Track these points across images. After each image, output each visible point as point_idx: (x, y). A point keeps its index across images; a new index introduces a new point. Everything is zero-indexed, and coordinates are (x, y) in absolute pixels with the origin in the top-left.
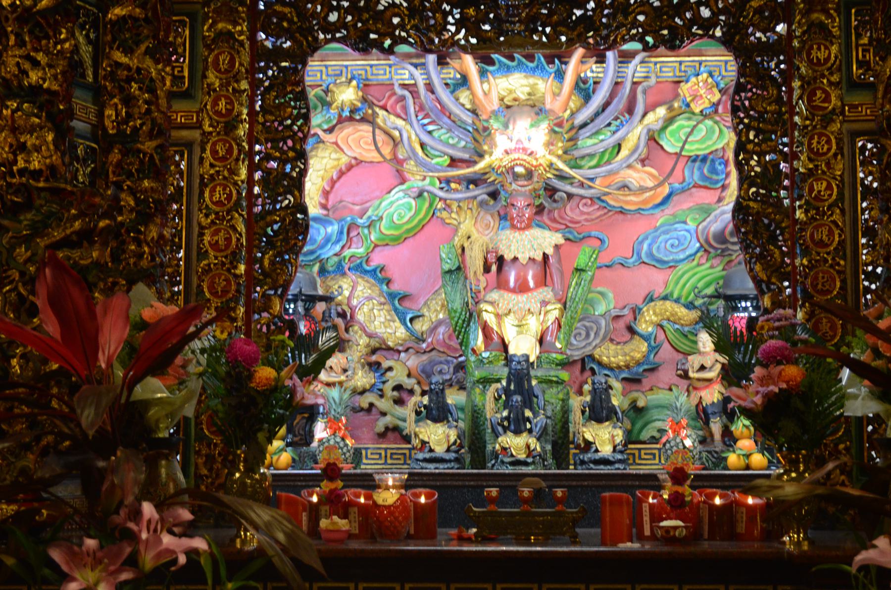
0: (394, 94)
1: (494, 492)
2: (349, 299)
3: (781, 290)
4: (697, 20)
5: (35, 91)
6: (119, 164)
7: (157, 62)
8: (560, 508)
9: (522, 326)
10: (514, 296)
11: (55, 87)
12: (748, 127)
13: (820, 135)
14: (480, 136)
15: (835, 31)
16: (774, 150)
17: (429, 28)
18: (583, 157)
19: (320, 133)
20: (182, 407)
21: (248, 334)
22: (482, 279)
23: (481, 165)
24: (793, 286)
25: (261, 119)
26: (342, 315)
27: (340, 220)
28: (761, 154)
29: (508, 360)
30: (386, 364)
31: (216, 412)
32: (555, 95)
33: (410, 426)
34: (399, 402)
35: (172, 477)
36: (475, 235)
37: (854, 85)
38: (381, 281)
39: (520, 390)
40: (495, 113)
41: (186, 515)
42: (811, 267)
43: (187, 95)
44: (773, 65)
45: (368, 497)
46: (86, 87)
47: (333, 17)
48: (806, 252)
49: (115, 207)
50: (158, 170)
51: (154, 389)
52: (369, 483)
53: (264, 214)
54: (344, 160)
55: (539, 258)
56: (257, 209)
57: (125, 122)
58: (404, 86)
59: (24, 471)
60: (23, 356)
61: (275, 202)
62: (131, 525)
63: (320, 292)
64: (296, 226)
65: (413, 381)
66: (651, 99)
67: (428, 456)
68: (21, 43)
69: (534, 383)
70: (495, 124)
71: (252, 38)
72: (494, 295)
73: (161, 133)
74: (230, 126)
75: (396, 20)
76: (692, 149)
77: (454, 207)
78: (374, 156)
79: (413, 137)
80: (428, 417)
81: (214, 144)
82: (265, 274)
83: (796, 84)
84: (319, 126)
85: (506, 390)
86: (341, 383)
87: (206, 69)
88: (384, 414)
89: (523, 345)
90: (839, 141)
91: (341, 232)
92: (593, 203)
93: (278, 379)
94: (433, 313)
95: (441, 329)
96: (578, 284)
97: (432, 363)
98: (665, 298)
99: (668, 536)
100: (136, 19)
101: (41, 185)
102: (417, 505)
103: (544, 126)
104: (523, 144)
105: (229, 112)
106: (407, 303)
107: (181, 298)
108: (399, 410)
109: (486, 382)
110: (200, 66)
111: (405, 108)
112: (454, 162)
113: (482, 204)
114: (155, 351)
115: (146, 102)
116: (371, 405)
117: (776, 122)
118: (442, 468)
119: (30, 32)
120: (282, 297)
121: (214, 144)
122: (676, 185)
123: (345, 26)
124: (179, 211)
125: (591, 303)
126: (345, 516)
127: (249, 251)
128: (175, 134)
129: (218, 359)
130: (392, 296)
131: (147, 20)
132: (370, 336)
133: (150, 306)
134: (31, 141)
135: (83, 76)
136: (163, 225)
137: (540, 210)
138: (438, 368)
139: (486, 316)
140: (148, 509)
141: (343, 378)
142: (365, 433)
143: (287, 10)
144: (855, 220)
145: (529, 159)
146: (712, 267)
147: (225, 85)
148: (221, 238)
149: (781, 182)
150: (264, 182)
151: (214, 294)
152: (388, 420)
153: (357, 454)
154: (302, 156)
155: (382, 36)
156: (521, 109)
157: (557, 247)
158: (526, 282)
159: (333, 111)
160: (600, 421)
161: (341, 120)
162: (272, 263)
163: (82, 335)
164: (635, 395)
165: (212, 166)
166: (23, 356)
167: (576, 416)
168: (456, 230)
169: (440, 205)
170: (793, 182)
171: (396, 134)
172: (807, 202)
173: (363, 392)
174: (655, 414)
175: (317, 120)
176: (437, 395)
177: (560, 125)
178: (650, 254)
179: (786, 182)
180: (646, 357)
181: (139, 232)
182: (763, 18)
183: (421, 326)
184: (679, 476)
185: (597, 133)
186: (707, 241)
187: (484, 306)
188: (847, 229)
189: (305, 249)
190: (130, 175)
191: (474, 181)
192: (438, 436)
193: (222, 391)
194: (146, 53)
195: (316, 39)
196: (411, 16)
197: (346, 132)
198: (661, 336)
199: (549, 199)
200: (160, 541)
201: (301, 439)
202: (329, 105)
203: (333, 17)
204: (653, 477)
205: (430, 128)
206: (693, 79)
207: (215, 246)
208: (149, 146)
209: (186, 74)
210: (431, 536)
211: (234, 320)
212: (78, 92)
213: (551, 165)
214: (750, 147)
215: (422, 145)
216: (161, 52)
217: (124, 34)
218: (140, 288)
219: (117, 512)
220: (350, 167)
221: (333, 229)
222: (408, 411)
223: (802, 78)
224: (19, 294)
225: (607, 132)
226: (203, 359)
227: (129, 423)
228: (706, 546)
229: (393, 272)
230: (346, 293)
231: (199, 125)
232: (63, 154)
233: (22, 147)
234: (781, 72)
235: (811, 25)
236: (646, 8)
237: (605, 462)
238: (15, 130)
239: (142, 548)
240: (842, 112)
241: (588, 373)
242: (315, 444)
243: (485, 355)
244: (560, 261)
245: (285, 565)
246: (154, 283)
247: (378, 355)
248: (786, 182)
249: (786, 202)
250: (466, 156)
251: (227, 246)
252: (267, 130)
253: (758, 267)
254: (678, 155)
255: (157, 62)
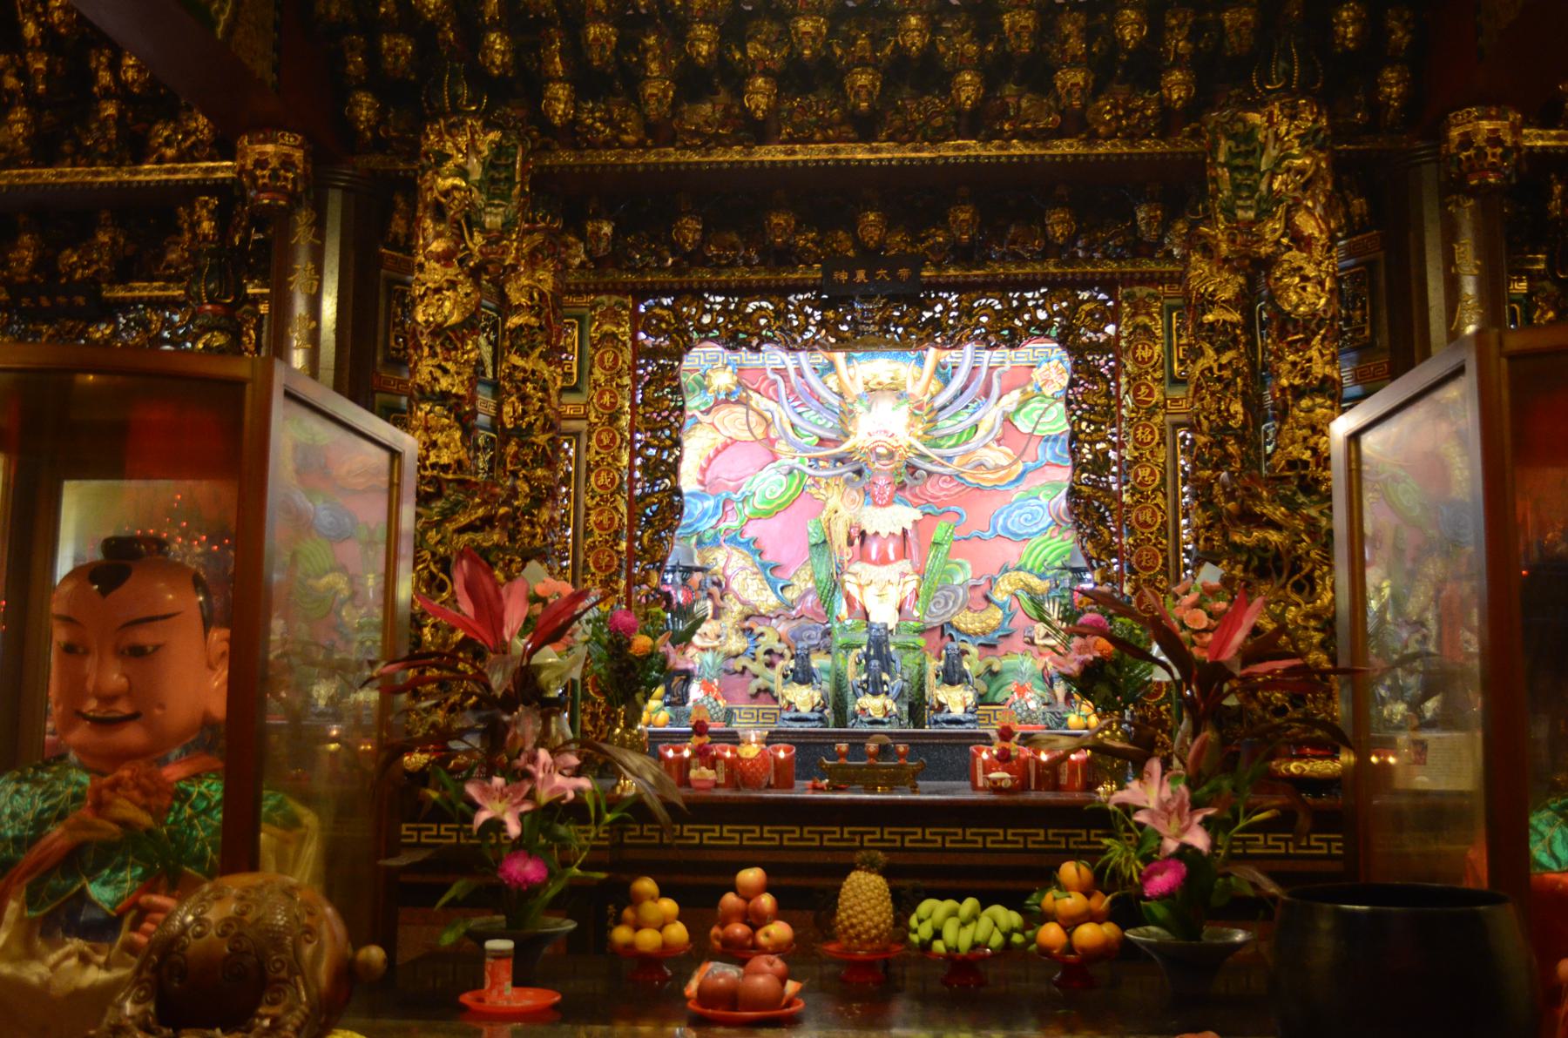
0: (767, 378)
1: (844, 747)
2: (724, 568)
3: (1109, 566)
4: (1034, 321)
5: (444, 397)
6: (516, 455)
7: (550, 364)
8: (902, 761)
9: (882, 594)
10: (875, 568)
11: (462, 392)
12: (1081, 419)
13: (1145, 426)
14: (845, 416)
15: (1159, 333)
16: (1103, 440)
17: (792, 329)
18: (942, 437)
19: (698, 414)
20: (570, 670)
21: (629, 604)
22: (847, 550)
23: (843, 448)
24: (1121, 563)
25: (641, 411)
26: (718, 584)
27: (716, 495)
28: (1093, 443)
29: (870, 627)
30: (758, 630)
31: (599, 675)
32: (916, 380)
33: (778, 687)
34: (770, 665)
35: (560, 732)
36: (842, 511)
37: (1176, 381)
38: (754, 552)
39: (879, 656)
40: (859, 397)
41: (573, 760)
42: (1136, 546)
43: (575, 389)
44: (1102, 362)
45: (733, 751)
46: (485, 383)
47: (706, 320)
48: (1132, 532)
49: (514, 493)
50: (548, 460)
51: (548, 655)
52: (733, 739)
53: (644, 496)
54: (720, 440)
55: (899, 532)
56: (638, 492)
57: (522, 417)
58: (776, 371)
59: (434, 725)
60: (434, 626)
61: (653, 485)
62: (530, 767)
63: (697, 563)
64: (672, 505)
65: (783, 646)
66: (1006, 382)
67: (794, 715)
68: (434, 355)
69: (892, 648)
70: (859, 408)
71: (634, 338)
72: (857, 567)
73: (552, 427)
74: (614, 418)
75: (763, 322)
76: (1043, 430)
77: (823, 483)
78: (746, 436)
79: (785, 418)
80: (794, 680)
81: (599, 434)
82: (644, 550)
83: (1123, 380)
84: (697, 408)
85: (867, 656)
86: (714, 649)
87: (592, 366)
88: (756, 676)
89: (884, 614)
90: (1162, 431)
91: (717, 507)
92: (952, 479)
93: (653, 647)
94: (802, 582)
95: (810, 598)
96: (935, 557)
97: (802, 629)
98: (1019, 569)
99: (995, 788)
100: (532, 327)
101: (450, 476)
102: (776, 759)
103: (905, 409)
104: (883, 426)
105: (613, 404)
106: (778, 573)
107: (569, 572)
108: (769, 673)
109: (848, 647)
110: (587, 363)
111: (776, 391)
112: (822, 442)
113: (847, 481)
114: (551, 626)
115: (540, 400)
116: (745, 668)
117: (1106, 414)
118: (806, 727)
119: (442, 344)
120: (659, 570)
121: (599, 434)
122: (1030, 464)
123: (717, 327)
124: (568, 494)
125: (951, 574)
126: (714, 767)
127: (630, 530)
128: (566, 425)
129: (601, 628)
130: (764, 566)
131: (541, 328)
132: (744, 603)
133: (539, 579)
134: (441, 438)
135: (484, 373)
136: (554, 509)
137: (902, 486)
138: (807, 634)
139: (848, 586)
140: (543, 754)
141: (716, 643)
142: (739, 694)
143: (665, 313)
144: (1176, 503)
145: (890, 440)
146: (1063, 540)
147: (609, 381)
148: (605, 518)
149: (1109, 470)
150: (644, 468)
151: (599, 568)
152: (759, 682)
153: (729, 714)
154: (677, 443)
155: (751, 335)
156: (883, 391)
157: (915, 522)
158: (886, 554)
159: (710, 396)
160: (952, 684)
161: (717, 403)
162: (651, 540)
163: (490, 612)
164: (990, 659)
165: (597, 453)
166: (434, 626)
167: (931, 680)
168: (823, 506)
169: (810, 481)
170: (1120, 469)
171: (768, 415)
172: (1133, 487)
173: (736, 656)
174: (1009, 677)
175: (694, 403)
176: (803, 659)
177: (920, 408)
178: (1005, 528)
179: (1115, 469)
180: (1001, 624)
181: (533, 515)
182: (1094, 320)
183: (790, 595)
184: (1006, 734)
185: (956, 414)
186: (1058, 516)
187: (846, 577)
188: (1170, 512)
189: (684, 522)
190: (525, 465)
191: (841, 460)
192: (803, 698)
193: (605, 657)
194: (541, 356)
195: (691, 339)
196: (777, 318)
197: (722, 414)
198: (1015, 604)
199: (909, 477)
200: (552, 780)
201: (677, 700)
202: (707, 388)
203: (706, 320)
204: (986, 736)
205: (800, 410)
206: (1045, 365)
207: (599, 525)
208: (541, 439)
209: (575, 370)
210: (790, 786)
211: (617, 592)
212: (479, 388)
213: (911, 446)
214: (1082, 436)
215: (793, 426)
216: (553, 354)
217: (521, 340)
218: (533, 565)
219: (518, 757)
220: (726, 446)
221: (709, 504)
222: (776, 674)
223: (1128, 375)
224: (431, 573)
225: (965, 414)
226: (589, 629)
227: (527, 686)
228: (1033, 796)
229: (767, 544)
230: (721, 564)
231: (586, 417)
232: (469, 449)
233: (434, 444)
234: (1111, 369)
235: (1137, 327)
236: (988, 311)
237: (957, 722)
238: (427, 429)
239: (539, 785)
240: (1165, 406)
241: (947, 639)
242: (690, 704)
243: (848, 622)
244: (918, 536)
245: (655, 805)
246: (546, 560)
247: (750, 622)
248: (1115, 469)
249: (1115, 487)
250: (833, 436)
251: (611, 526)
252: (647, 420)
253: (1089, 546)
254: (1031, 434)
255: (550, 364)
